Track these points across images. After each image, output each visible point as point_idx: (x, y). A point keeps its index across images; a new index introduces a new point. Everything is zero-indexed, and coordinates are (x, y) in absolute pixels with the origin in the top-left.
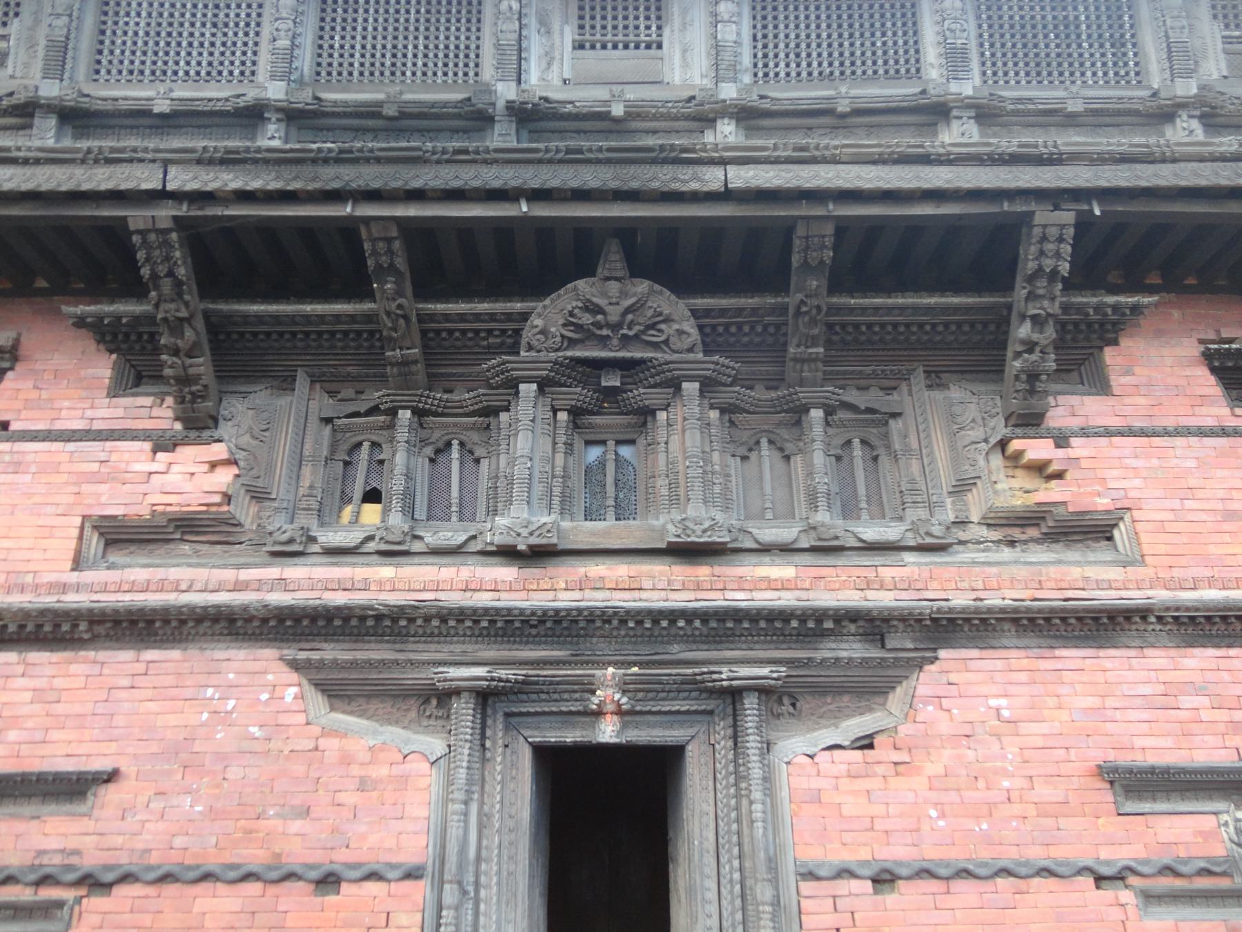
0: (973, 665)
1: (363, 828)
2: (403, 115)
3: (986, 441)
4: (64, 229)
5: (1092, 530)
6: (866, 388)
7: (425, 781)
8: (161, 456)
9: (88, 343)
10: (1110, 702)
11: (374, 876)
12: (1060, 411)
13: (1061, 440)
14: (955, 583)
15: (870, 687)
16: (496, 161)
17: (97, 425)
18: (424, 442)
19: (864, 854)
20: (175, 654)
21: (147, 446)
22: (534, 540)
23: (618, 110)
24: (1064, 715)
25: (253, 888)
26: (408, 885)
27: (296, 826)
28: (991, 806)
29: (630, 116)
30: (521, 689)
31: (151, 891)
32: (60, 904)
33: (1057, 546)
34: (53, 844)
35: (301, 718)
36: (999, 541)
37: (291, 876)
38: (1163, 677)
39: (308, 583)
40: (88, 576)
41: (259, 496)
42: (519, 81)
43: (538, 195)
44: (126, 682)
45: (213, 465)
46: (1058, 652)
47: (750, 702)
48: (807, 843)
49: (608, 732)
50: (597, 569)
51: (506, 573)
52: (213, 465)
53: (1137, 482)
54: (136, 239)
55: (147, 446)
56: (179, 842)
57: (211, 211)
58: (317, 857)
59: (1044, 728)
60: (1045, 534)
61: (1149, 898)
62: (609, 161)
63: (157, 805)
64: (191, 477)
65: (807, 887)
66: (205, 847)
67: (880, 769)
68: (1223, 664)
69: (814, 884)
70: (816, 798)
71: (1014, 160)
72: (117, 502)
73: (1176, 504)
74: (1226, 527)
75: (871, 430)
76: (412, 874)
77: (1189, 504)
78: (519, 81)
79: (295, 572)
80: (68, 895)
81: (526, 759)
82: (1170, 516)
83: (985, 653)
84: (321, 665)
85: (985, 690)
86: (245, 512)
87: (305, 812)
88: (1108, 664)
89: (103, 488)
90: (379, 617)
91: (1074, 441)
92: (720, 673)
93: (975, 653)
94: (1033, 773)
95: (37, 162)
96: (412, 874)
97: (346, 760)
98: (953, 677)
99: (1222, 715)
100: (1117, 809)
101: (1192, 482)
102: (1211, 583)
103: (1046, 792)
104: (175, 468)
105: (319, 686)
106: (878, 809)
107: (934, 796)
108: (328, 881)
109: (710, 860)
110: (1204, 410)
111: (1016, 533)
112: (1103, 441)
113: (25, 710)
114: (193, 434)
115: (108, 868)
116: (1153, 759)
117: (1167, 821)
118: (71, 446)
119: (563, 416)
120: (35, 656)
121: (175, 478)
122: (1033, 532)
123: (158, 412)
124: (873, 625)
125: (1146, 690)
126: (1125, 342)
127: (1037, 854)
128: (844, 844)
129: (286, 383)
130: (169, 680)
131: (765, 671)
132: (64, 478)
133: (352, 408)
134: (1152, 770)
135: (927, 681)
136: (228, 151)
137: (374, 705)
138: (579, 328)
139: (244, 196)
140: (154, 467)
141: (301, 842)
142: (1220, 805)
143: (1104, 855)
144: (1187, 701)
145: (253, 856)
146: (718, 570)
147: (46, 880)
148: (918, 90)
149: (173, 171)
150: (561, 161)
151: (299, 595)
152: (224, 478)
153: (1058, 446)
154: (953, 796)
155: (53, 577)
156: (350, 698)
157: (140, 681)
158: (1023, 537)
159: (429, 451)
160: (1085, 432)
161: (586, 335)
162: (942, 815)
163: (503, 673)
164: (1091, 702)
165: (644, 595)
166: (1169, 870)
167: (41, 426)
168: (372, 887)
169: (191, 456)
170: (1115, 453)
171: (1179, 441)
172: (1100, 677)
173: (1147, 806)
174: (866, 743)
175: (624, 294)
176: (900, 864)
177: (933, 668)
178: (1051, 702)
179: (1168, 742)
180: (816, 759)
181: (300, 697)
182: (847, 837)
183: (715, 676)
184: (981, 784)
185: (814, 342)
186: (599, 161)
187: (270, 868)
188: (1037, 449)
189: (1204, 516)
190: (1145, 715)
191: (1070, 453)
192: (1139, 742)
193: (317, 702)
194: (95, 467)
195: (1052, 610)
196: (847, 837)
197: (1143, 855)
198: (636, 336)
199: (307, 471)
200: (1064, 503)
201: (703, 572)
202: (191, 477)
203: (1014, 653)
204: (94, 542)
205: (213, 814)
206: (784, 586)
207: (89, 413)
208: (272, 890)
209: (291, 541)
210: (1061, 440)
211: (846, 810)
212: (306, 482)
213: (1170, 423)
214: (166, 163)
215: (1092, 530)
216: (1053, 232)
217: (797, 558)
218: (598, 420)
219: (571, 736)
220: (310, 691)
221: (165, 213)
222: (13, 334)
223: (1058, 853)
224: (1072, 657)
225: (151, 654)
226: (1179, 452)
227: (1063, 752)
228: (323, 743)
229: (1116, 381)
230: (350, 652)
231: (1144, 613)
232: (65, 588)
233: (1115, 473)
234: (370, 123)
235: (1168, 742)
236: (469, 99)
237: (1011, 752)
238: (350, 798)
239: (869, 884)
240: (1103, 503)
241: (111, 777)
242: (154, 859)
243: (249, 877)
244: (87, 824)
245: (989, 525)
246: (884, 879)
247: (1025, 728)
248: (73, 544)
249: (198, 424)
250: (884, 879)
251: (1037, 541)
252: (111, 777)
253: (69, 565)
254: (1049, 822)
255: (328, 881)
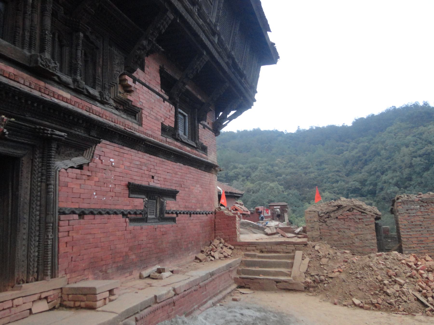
10: (131, 166)
46: (125, 148)
60: (125, 109)
61: (132, 220)
67: (84, 177)
69: (64, 216)
75: (343, 126)
85: (109, 155)
88: (133, 154)
92: (48, 131)
93: (108, 142)
94: (116, 183)
100: (129, 195)
109: (27, 207)
128: (72, 202)
162: (96, 195)
174: (80, 167)
178: (121, 162)
180: (68, 171)
182: (74, 200)
183: (46, 131)
184: (105, 185)
196: (74, 200)
200: (132, 101)
203: (116, 145)
211: (75, 191)
227: (122, 178)
245: (114, 101)
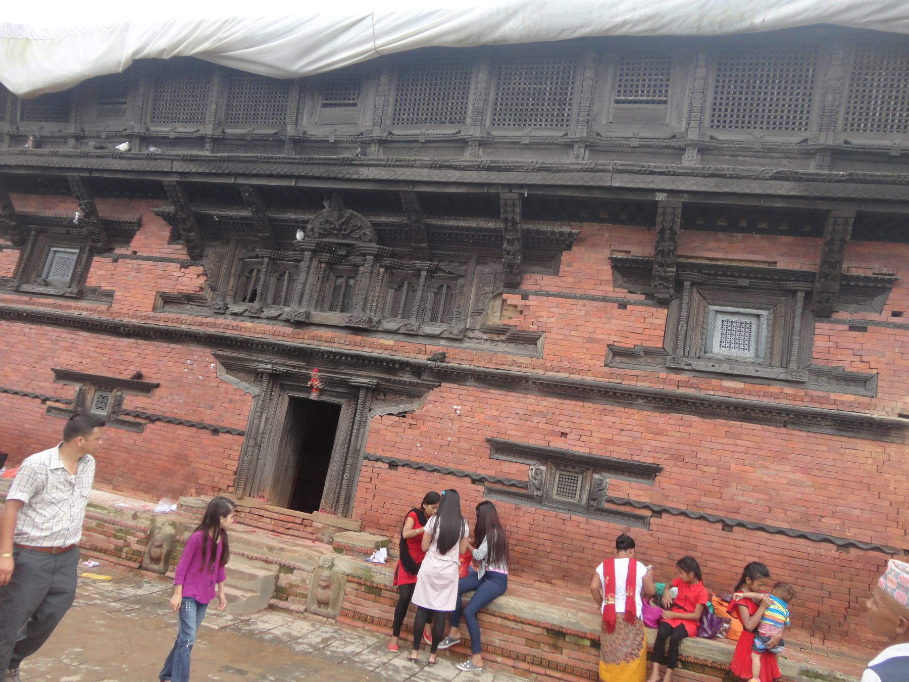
0: (453, 391)
1: (228, 416)
2: (253, 140)
3: (493, 292)
4: (142, 182)
5: (527, 339)
6: (453, 262)
7: (251, 404)
8: (183, 270)
9: (160, 220)
11: (228, 432)
12: (531, 282)
13: (525, 297)
14: (461, 357)
15: (413, 393)
16: (283, 163)
17: (164, 256)
18: (275, 271)
19: (389, 455)
20: (179, 346)
21: (178, 265)
22: (297, 319)
23: (332, 140)
24: (482, 416)
25: (193, 429)
26: (238, 437)
27: (209, 412)
28: (441, 446)
29: (336, 142)
30: (287, 375)
31: (165, 425)
32: (141, 424)
33: (512, 345)
34: (140, 405)
35: (214, 375)
36: (487, 340)
37: (204, 428)
38: (530, 407)
39: (225, 326)
40: (157, 315)
41: (213, 289)
42: (296, 125)
43: (299, 177)
44: (164, 354)
45: (199, 275)
47: (362, 394)
48: (370, 445)
49: (314, 396)
50: (320, 332)
51: (289, 330)
52: (199, 275)
53: (553, 320)
54: (166, 188)
55: (178, 265)
56: (175, 411)
57: (190, 179)
58: (214, 423)
59: (471, 420)
62: (324, 164)
63: (170, 398)
64: (190, 280)
65: (365, 462)
66: (181, 413)
67: (404, 425)
68: (559, 406)
70: (378, 431)
71: (489, 169)
72: (169, 288)
73: (567, 332)
74: (587, 345)
76: (241, 434)
77: (573, 333)
78: (296, 125)
79: (221, 320)
80: (143, 421)
81: (287, 400)
82: (562, 337)
83: (460, 387)
84: (227, 357)
86: (208, 294)
87: (212, 408)
89: (164, 281)
90: (241, 342)
91: (531, 297)
93: (456, 386)
95: (133, 159)
96: (241, 434)
97: (226, 392)
98: (443, 395)
99: (549, 427)
101: (579, 322)
102: (566, 370)
103: (463, 445)
104: (187, 275)
105: (223, 364)
106: (399, 440)
107: (420, 438)
108: (215, 431)
110: (600, 288)
111: (495, 337)
112: (544, 298)
113: (135, 360)
114: (193, 262)
115: (154, 415)
116: (512, 440)
117: (508, 464)
118: (155, 263)
119: (323, 265)
120: (140, 341)
121: (185, 280)
122: (503, 337)
123: (180, 251)
124: (417, 369)
125: (521, 412)
126: (574, 249)
127: (452, 467)
129: (227, 242)
130: (177, 356)
131: (367, 381)
132: (151, 276)
133: (251, 255)
134: (505, 443)
135: (432, 395)
136: (192, 156)
137: (241, 374)
138: (325, 230)
139: (197, 174)
140: (181, 274)
141: (209, 417)
142: (533, 462)
143: (478, 472)
144: (536, 419)
145: (194, 419)
146: (365, 338)
147: (137, 416)
148: (456, 131)
149: (175, 163)
150: (306, 164)
151: (218, 330)
152: (201, 281)
153: (523, 298)
154: (428, 440)
155: (146, 314)
156: (233, 370)
157: (169, 355)
158: (497, 339)
159: (277, 275)
160: (536, 293)
161: (327, 233)
163: (280, 368)
164: (496, 413)
165: (334, 345)
166: (499, 482)
167: (146, 254)
168: (228, 435)
169: (194, 270)
170: (548, 304)
171: (581, 302)
172: (503, 403)
173: (501, 457)
174: (402, 415)
175: (340, 217)
176: (400, 460)
177: (438, 389)
178: (479, 410)
179: (521, 434)
181: (215, 368)
182: (385, 448)
185: (422, 241)
186: (321, 164)
187: (198, 424)
188: (513, 299)
189: (577, 339)
190: (516, 422)
191: (527, 303)
192: (509, 432)
193: (222, 371)
194: (161, 272)
195: (489, 373)
197: (493, 475)
198: (348, 234)
199: (232, 279)
201: (359, 338)
202: (190, 280)
204: (160, 302)
205: (185, 403)
206: (386, 348)
207: (162, 250)
208: (200, 431)
209: (220, 309)
210: (525, 297)
212: (231, 284)
213: (579, 292)
214: (172, 160)
215: (527, 339)
216: (510, 202)
217: (397, 337)
218: (340, 267)
219: (302, 395)
220: (220, 366)
221: (175, 179)
222: (137, 216)
223: (461, 468)
224: (495, 393)
225: (173, 346)
226: (578, 307)
228: (220, 385)
229: (564, 268)
230: (233, 351)
231: (526, 379)
232: (148, 318)
233: (544, 314)
234: (242, 142)
235: (521, 434)
236: (276, 133)
237: (456, 427)
238: (226, 405)
239: (387, 466)
240: (534, 328)
241: (158, 386)
242: (167, 415)
243: (192, 426)
244: (149, 401)
246: (393, 465)
247: (464, 418)
248: (153, 302)
249: (196, 256)
250: (393, 465)
251: (503, 341)
252: (158, 386)
253: (151, 309)
254: (462, 456)
255: (215, 431)
